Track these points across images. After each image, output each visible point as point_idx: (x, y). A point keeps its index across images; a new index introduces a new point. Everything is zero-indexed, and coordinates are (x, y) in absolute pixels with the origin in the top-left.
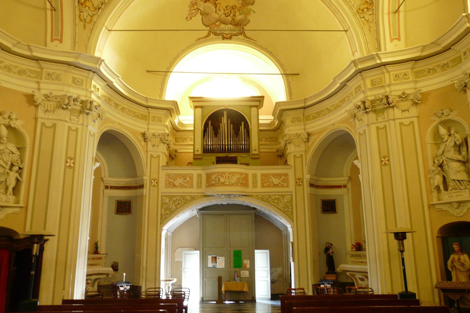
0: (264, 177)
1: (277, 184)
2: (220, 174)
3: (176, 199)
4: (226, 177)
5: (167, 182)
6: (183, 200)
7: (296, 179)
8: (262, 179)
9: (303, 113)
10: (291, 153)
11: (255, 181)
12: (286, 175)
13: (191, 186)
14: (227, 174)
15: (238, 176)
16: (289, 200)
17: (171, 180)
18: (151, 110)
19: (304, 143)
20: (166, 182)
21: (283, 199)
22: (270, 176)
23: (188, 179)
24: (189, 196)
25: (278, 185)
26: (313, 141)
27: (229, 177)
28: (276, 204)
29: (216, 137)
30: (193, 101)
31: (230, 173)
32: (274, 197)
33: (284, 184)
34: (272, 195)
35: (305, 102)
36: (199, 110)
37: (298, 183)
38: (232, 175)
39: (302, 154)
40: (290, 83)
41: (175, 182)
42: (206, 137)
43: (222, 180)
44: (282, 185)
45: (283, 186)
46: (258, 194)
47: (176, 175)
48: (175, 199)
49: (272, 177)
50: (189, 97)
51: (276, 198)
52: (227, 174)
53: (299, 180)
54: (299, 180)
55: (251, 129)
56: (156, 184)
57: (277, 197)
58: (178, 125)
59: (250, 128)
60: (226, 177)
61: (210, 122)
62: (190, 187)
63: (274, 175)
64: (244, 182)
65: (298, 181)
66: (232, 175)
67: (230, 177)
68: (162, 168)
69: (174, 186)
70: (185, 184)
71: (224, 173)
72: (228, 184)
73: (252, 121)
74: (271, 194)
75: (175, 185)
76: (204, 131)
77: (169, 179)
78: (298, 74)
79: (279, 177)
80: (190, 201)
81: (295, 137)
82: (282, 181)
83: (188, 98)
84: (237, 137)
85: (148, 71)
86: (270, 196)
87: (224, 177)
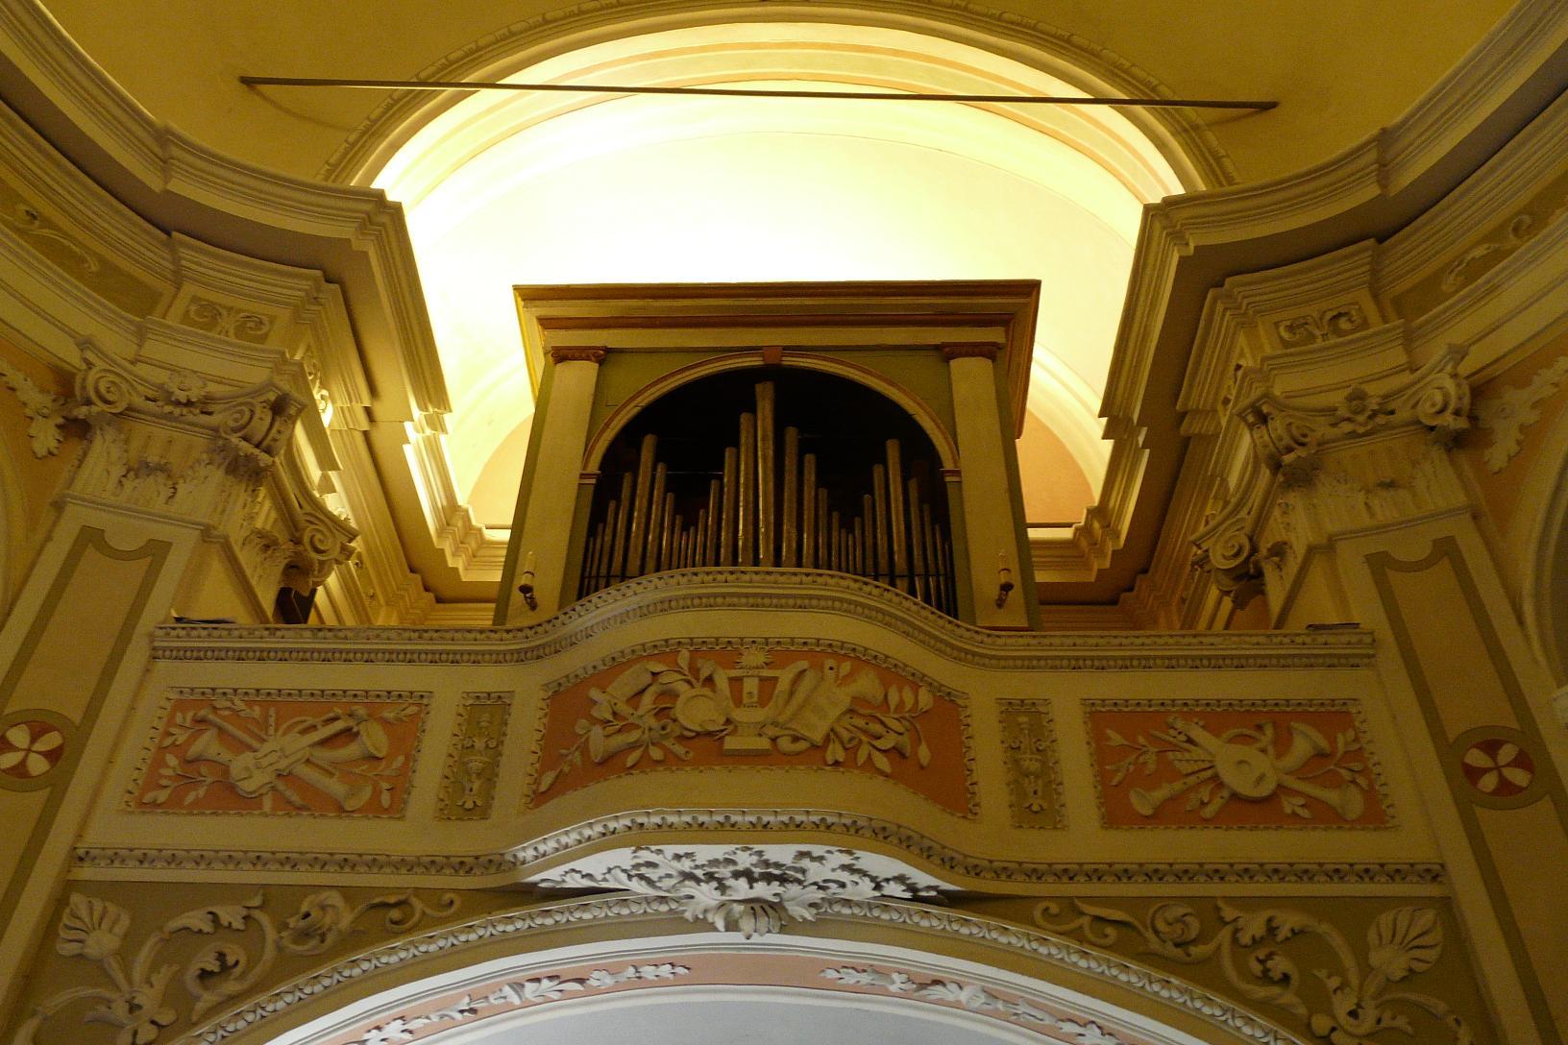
0: (1116, 739)
1: (1266, 790)
2: (684, 658)
3: (207, 928)
4: (736, 682)
5: (172, 760)
6: (271, 934)
7: (1448, 750)
8: (1102, 755)
9: (1374, 272)
10: (1342, 547)
11: (1031, 764)
12: (1333, 716)
13: (391, 803)
14: (754, 658)
15: (867, 684)
16: (1432, 955)
17: (206, 744)
18: (194, 257)
19: (1437, 454)
20: (159, 762)
21: (1362, 953)
22: (1180, 724)
23: (375, 738)
24: (348, 893)
25: (1270, 799)
26: (1531, 417)
27: (768, 684)
28: (1287, 997)
29: (685, 528)
30: (546, 323)
31: (780, 652)
32: (1254, 926)
33: (1332, 796)
34: (1230, 900)
35: (1384, 171)
36: (581, 376)
37: (1489, 782)
38: (803, 664)
39: (1451, 540)
40: (1218, 159)
41: (239, 765)
42: (609, 531)
43: (697, 711)
44: (1311, 802)
45: (1327, 817)
46: (1080, 888)
47: (266, 698)
48: (197, 920)
49: (1198, 733)
50: (516, 288)
51: (1284, 932)
52: (754, 658)
53: (1491, 747)
54: (1491, 747)
55: (957, 473)
56: (38, 765)
57: (1289, 921)
58: (441, 532)
59: (948, 465)
60: (736, 682)
61: (649, 443)
62: (374, 809)
63: (1220, 717)
64: (924, 753)
65: (1477, 758)
66: (803, 664)
67: (783, 684)
68: (152, 637)
69: (229, 797)
70: (335, 787)
71: (728, 651)
72: (764, 744)
73: (960, 430)
74: (1215, 889)
75: (232, 788)
76: (598, 487)
77: (194, 737)
78: (1273, 105)
79: (1269, 731)
80: (354, 940)
81: (1347, 427)
82: (1302, 772)
83: (511, 292)
84: (851, 530)
85: (249, 82)
86: (1210, 912)
87: (722, 680)
